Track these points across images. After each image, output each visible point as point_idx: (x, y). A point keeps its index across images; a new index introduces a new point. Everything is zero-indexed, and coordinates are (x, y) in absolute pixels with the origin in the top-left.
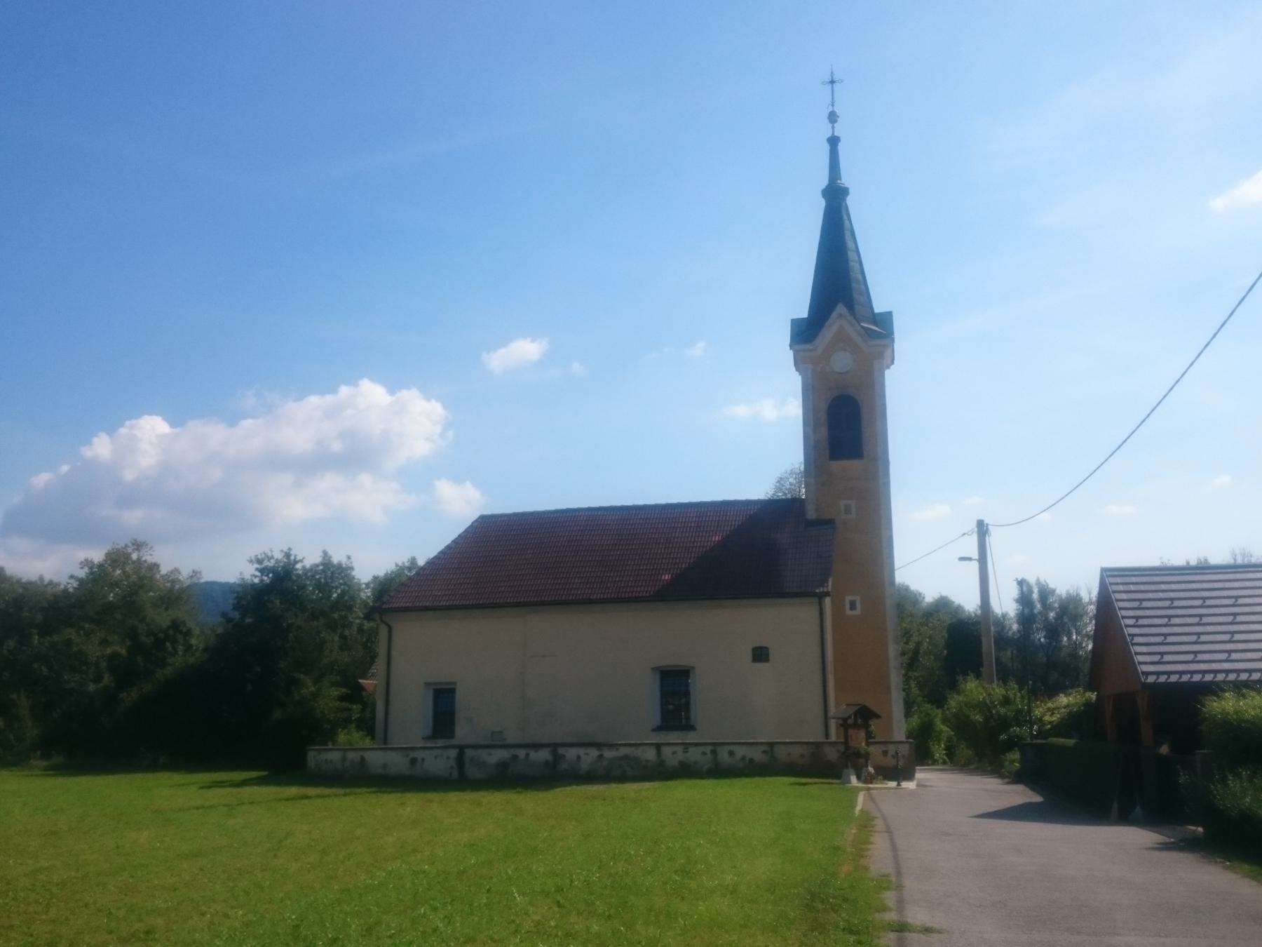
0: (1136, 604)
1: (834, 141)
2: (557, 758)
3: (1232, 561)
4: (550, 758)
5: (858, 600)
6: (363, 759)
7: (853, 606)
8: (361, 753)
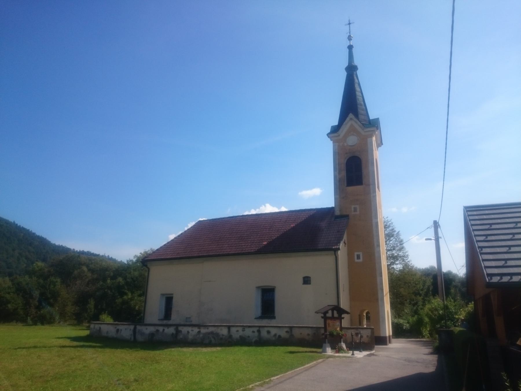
0: (487, 227)
1: (350, 47)
2: (178, 332)
4: (174, 332)
5: (361, 254)
6: (100, 328)
7: (358, 257)
8: (100, 325)
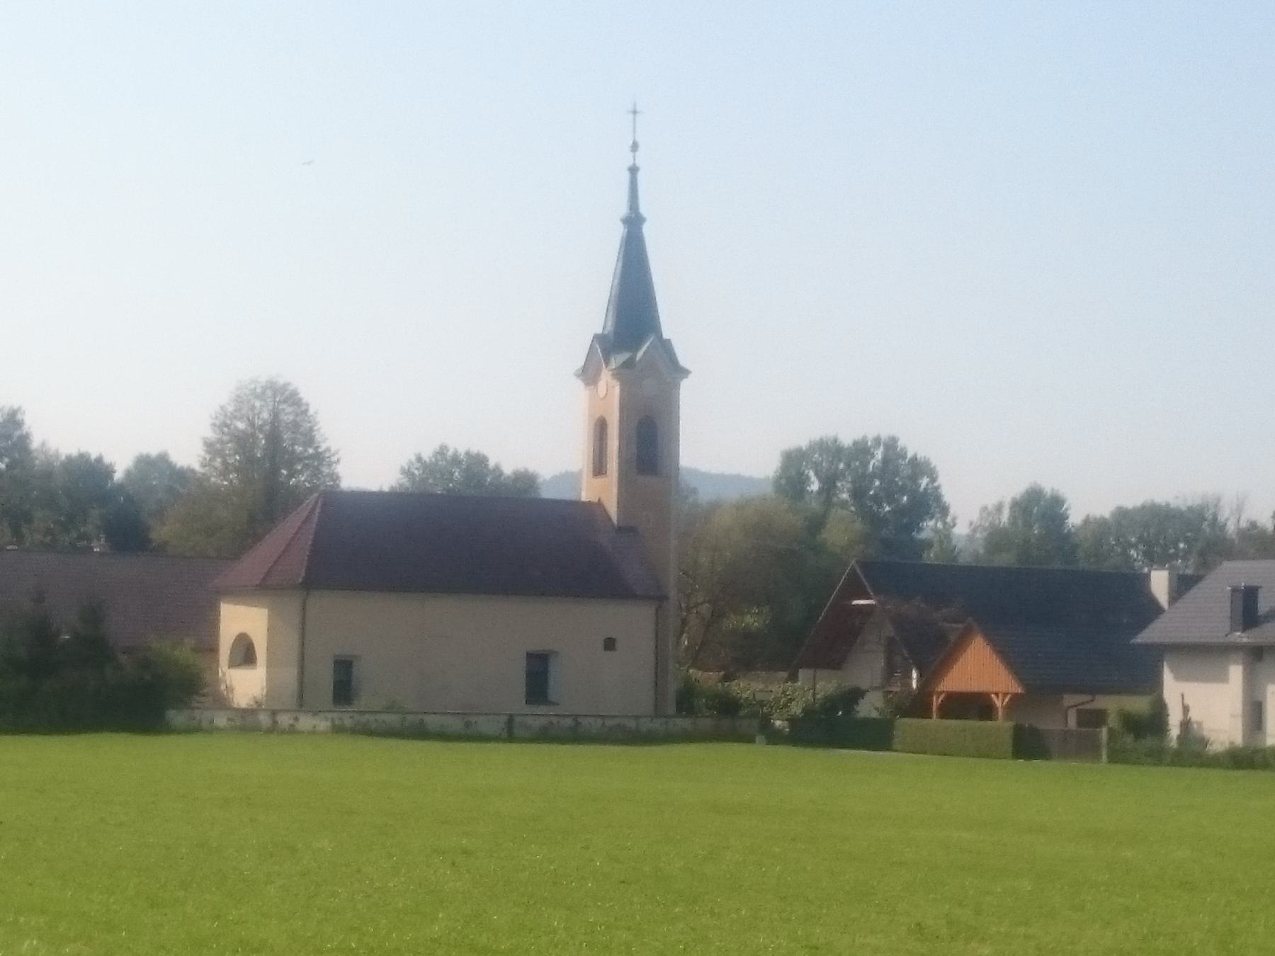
1: (634, 170)
2: (578, 724)
3: (546, 438)
